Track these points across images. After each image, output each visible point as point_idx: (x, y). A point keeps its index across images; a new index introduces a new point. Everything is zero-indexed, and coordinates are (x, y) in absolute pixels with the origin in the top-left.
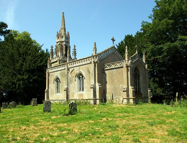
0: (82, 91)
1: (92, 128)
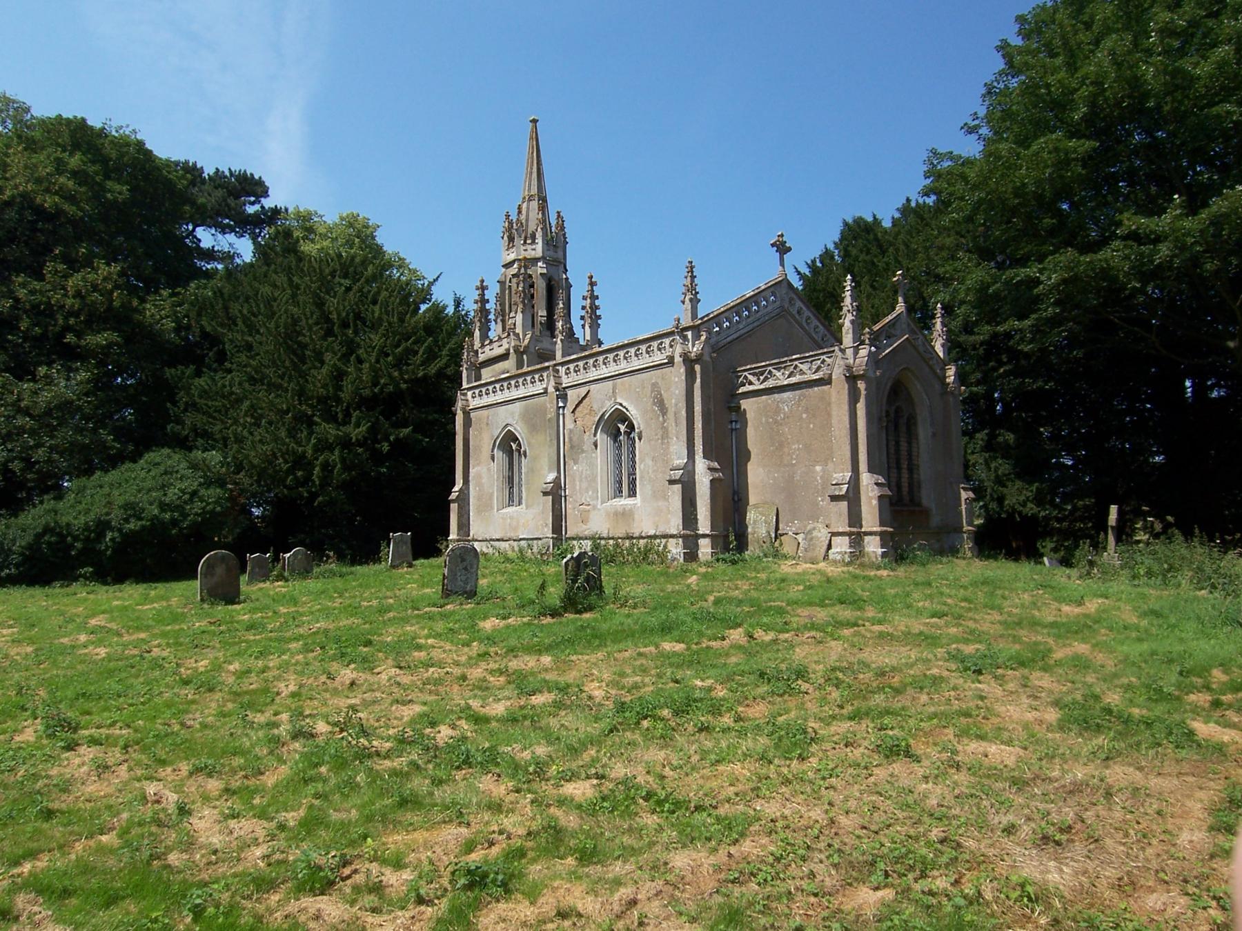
0: (630, 496)
1: (677, 682)
